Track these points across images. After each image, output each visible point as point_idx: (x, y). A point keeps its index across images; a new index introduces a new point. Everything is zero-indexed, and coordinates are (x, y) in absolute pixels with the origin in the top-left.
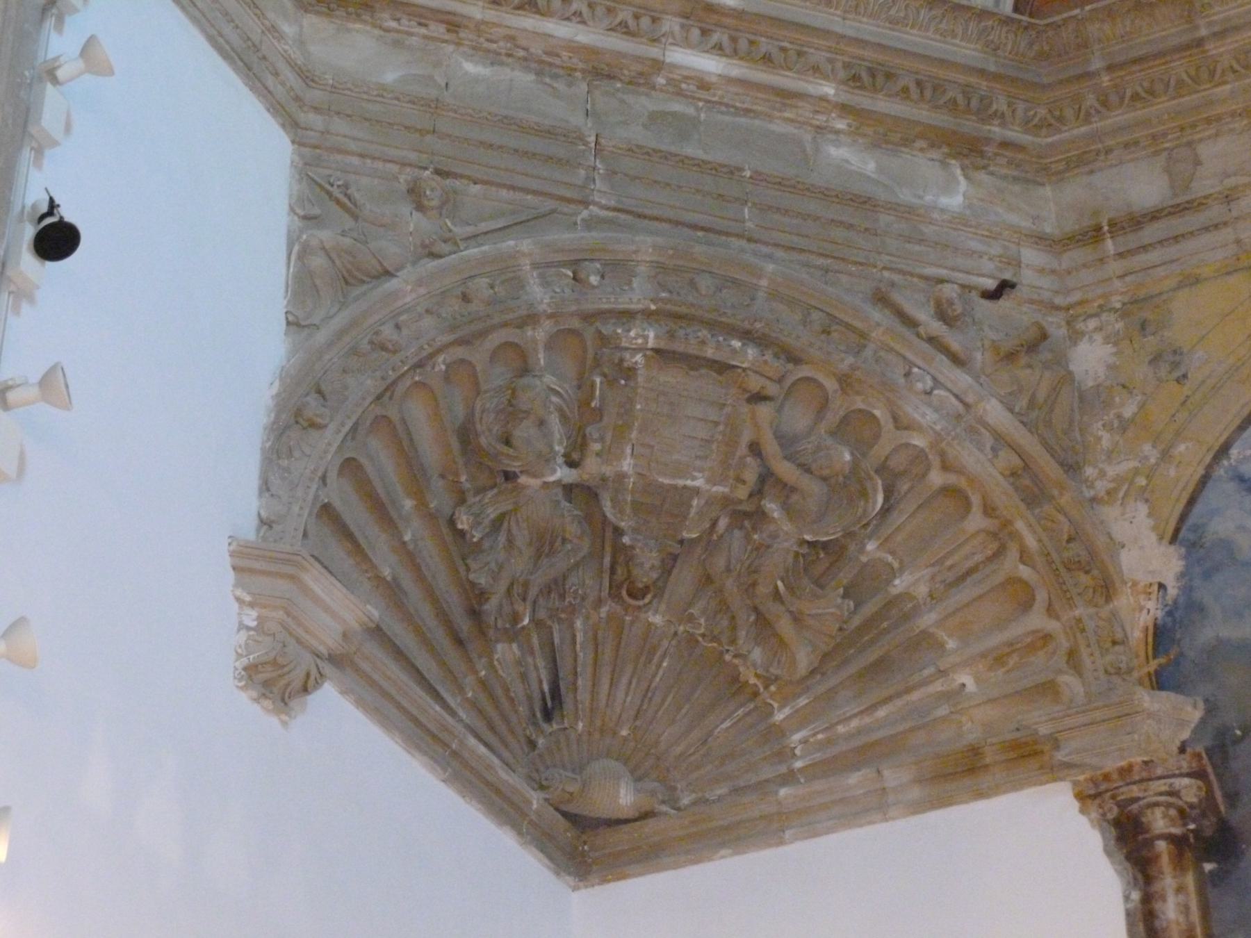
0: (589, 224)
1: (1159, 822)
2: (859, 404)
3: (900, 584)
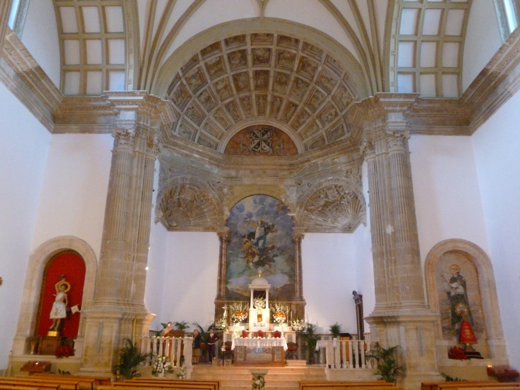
0: (185, 174)
1: (224, 238)
3: (204, 210)
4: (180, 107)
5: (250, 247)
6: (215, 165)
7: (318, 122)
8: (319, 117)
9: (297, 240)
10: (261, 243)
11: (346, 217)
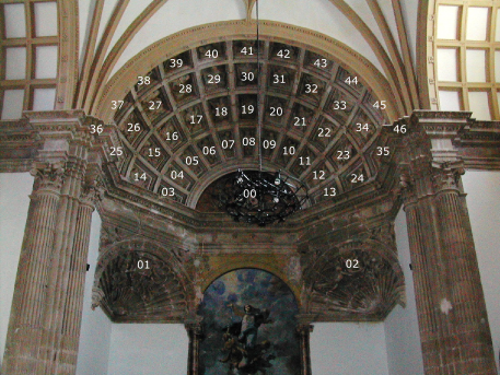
7: (328, 164)
9: (303, 333)
10: (250, 338)
11: (373, 298)
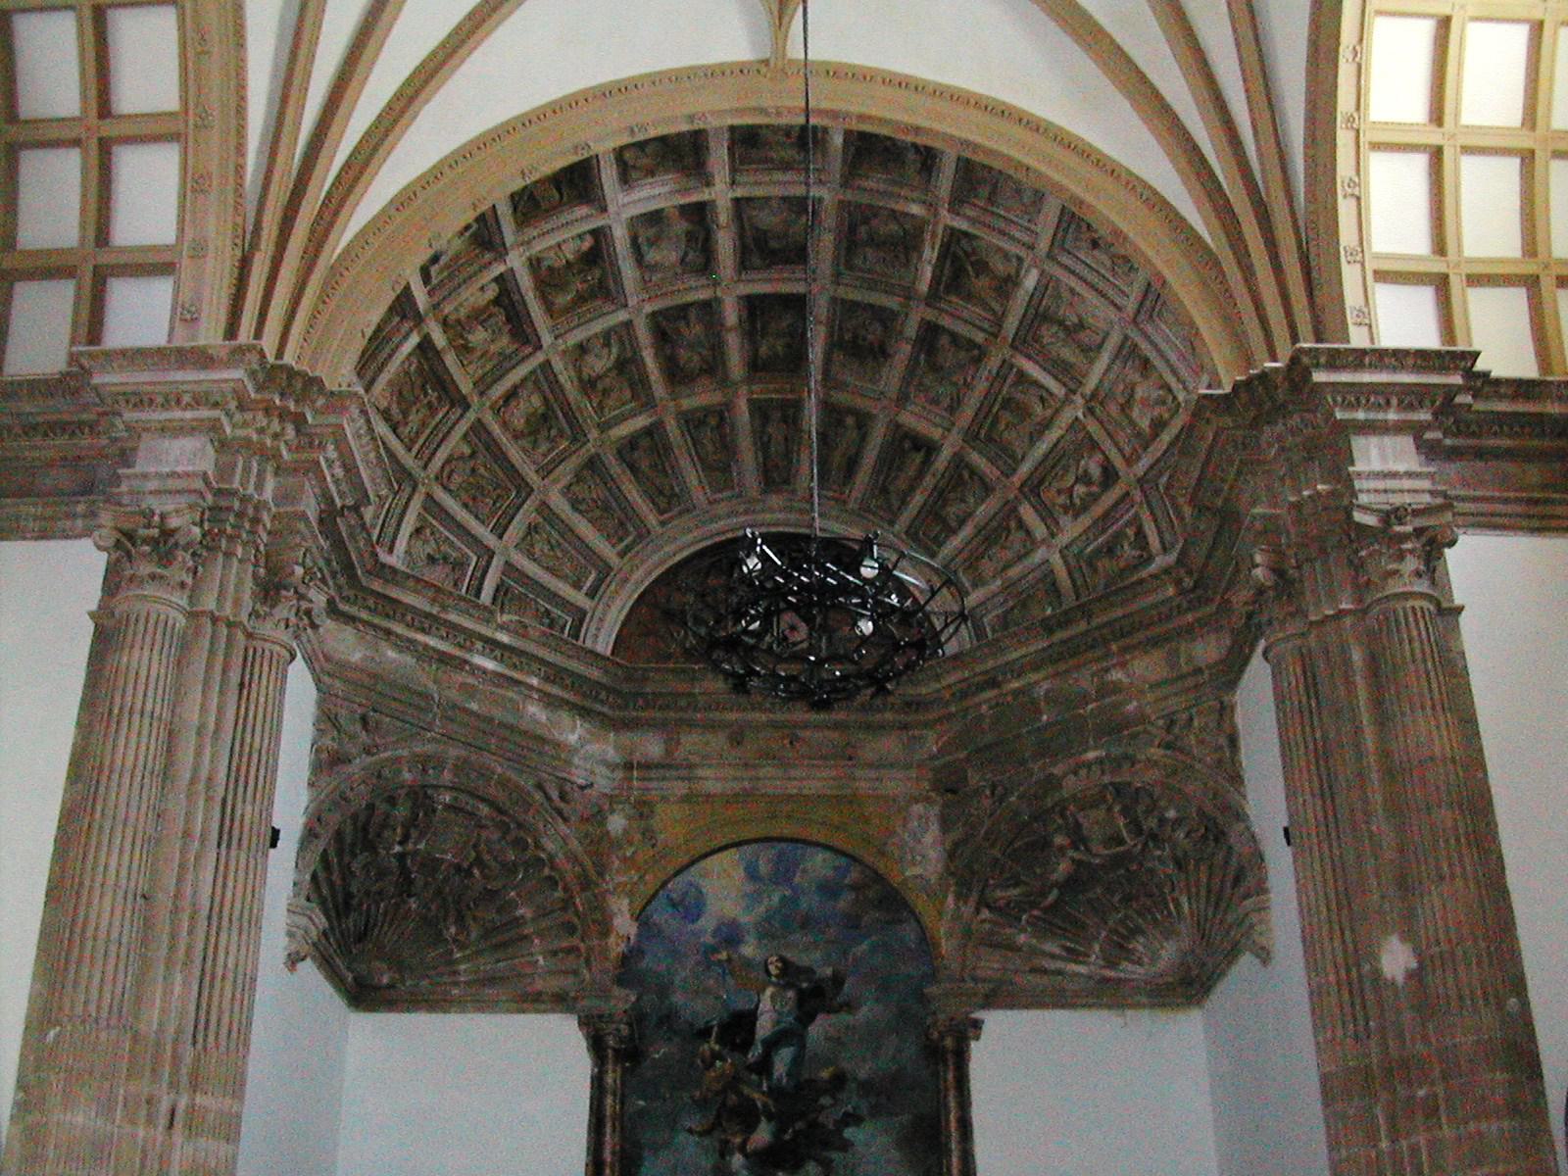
2: (522, 834)
3: (520, 912)
4: (417, 447)
5: (733, 1083)
6: (574, 708)
7: (1027, 513)
8: (1033, 488)
9: (949, 1042)
11: (1169, 934)
